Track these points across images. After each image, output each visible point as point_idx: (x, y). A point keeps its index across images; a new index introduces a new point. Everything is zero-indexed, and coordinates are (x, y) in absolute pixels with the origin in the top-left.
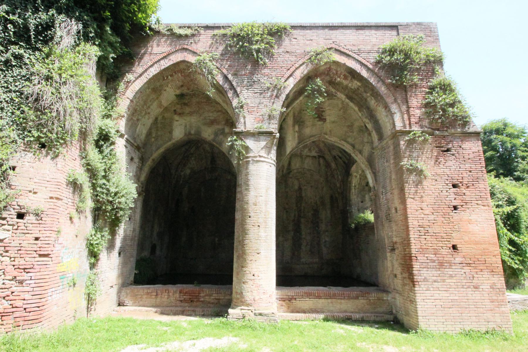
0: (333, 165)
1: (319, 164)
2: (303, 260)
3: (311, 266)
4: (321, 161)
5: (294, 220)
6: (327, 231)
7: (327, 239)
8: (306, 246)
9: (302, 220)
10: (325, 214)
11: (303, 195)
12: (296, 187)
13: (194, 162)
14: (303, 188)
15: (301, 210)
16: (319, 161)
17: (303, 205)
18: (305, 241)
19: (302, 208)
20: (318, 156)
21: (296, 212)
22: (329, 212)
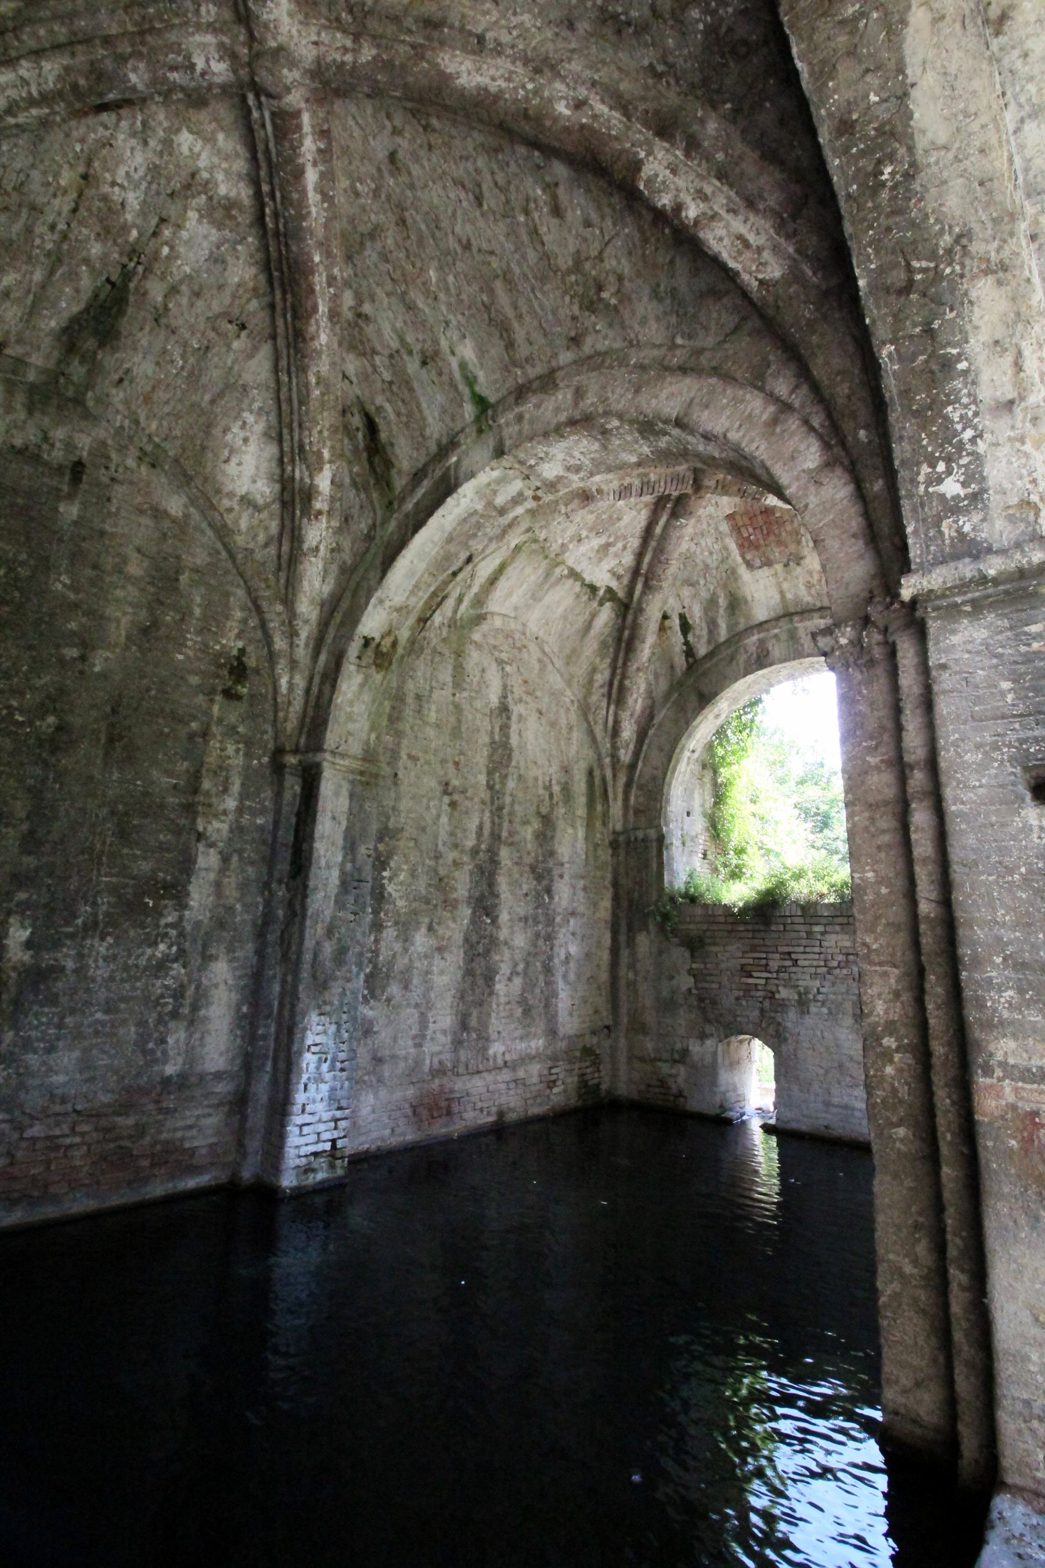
0: (646, 650)
1: (588, 626)
2: (496, 1049)
3: (521, 1073)
4: (606, 614)
5: (475, 852)
6: (573, 914)
7: (573, 949)
8: (510, 979)
9: (505, 854)
10: (572, 843)
11: (514, 741)
12: (494, 699)
14: (516, 709)
15: (501, 808)
16: (593, 616)
17: (511, 784)
18: (507, 953)
19: (508, 800)
20: (609, 590)
21: (487, 814)
22: (581, 833)
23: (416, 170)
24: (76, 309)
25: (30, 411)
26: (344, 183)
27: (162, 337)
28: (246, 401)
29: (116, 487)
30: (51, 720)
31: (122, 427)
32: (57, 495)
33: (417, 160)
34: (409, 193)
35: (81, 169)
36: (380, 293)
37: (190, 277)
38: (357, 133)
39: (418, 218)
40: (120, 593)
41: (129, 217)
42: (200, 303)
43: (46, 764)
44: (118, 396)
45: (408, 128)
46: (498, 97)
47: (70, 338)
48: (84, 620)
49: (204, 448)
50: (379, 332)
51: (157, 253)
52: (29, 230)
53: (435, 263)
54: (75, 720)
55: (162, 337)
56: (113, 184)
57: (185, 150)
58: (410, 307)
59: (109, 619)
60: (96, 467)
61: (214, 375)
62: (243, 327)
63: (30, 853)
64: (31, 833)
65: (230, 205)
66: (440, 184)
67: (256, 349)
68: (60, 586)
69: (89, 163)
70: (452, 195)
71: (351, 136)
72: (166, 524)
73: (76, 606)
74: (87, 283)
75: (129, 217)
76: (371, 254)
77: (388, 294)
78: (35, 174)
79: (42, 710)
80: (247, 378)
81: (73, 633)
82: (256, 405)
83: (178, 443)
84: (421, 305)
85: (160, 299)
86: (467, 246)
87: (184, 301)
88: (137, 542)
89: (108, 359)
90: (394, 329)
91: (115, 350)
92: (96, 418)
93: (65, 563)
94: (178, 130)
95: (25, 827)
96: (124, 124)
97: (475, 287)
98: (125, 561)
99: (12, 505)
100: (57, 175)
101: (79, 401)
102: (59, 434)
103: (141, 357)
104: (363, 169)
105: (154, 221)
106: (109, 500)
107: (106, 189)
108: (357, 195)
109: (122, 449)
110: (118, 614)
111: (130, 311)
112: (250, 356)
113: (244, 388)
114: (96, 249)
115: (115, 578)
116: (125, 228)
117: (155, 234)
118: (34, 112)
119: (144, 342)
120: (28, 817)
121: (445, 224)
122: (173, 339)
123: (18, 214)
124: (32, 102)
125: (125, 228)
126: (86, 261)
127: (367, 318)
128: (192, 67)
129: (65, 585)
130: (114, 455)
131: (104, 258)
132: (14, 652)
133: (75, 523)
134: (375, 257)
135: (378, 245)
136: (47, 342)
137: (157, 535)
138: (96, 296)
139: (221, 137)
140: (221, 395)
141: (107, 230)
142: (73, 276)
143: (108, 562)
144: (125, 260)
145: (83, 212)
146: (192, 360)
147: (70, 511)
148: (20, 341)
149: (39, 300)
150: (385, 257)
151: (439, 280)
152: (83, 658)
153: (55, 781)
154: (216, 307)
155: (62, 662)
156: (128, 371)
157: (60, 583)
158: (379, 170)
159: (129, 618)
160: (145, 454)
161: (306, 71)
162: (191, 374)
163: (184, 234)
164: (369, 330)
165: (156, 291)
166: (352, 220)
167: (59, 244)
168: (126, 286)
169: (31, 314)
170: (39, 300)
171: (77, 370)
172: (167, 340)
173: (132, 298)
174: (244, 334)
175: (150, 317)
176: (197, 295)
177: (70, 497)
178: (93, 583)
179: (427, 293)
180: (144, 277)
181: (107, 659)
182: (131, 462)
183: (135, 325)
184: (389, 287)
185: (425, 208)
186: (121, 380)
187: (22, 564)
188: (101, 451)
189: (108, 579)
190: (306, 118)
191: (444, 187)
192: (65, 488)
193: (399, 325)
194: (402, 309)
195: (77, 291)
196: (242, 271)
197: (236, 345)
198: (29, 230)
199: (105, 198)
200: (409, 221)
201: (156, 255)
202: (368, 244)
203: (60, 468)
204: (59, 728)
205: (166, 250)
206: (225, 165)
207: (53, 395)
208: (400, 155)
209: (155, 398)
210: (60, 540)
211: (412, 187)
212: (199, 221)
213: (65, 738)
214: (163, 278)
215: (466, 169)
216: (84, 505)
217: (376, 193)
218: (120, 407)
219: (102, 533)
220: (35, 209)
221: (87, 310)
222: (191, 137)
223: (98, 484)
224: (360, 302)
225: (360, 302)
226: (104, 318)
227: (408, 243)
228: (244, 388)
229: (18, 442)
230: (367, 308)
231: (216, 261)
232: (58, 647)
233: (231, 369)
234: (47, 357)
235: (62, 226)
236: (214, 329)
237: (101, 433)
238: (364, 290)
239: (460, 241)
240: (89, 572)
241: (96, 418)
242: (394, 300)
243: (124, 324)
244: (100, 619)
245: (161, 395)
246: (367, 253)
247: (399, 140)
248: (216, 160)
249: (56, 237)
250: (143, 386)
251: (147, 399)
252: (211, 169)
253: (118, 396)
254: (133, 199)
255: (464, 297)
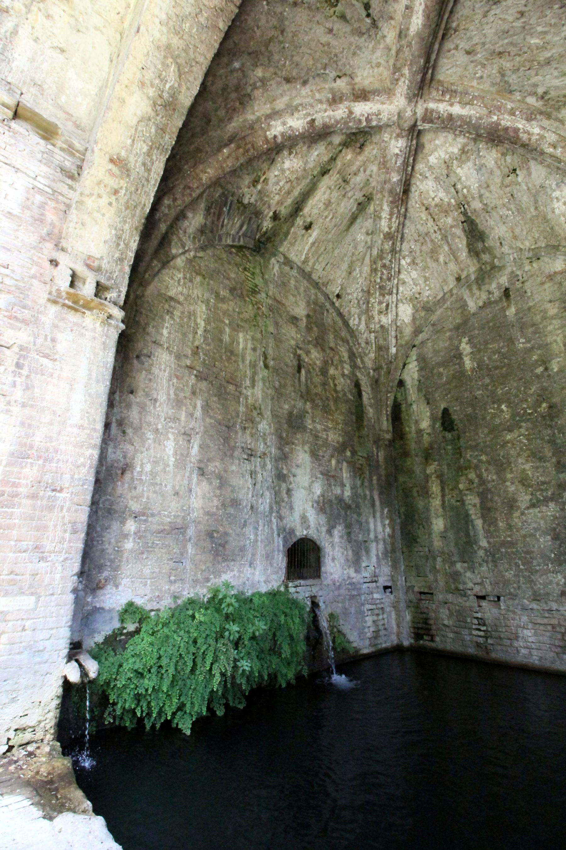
13: (414, 274)
23: (476, 40)
24: (465, 242)
25: (480, 289)
26: (475, 83)
27: (495, 214)
28: (549, 190)
29: (526, 284)
30: (544, 405)
31: (515, 259)
32: (503, 310)
33: (470, 38)
34: (487, 46)
35: (424, 208)
36: (534, 80)
37: (480, 186)
38: (454, 70)
39: (501, 43)
40: (550, 328)
41: (446, 200)
42: (492, 188)
43: (551, 426)
44: (506, 249)
45: (455, 41)
46: (426, 6)
47: (474, 252)
48: (539, 352)
49: (552, 228)
50: (557, 88)
51: (464, 195)
52: (432, 241)
53: (528, 37)
54: (556, 400)
55: (495, 214)
56: (433, 199)
57: (435, 161)
58: (548, 62)
59: (551, 343)
60: (514, 284)
61: (525, 199)
62: (515, 170)
63: (562, 472)
64: (559, 462)
65: (463, 151)
66: (485, 27)
67: (528, 169)
68: (521, 345)
69: (423, 204)
70: (492, 19)
71: (455, 73)
72: (558, 278)
73: (533, 348)
74: (459, 232)
75: (446, 200)
76: (513, 79)
77: (537, 75)
78: (419, 226)
79: (538, 403)
80: (538, 182)
81: (536, 361)
82: (554, 186)
83: (542, 238)
84: (549, 55)
85: (480, 205)
86: (522, 14)
87: (487, 194)
88: (548, 298)
89: (490, 243)
90: (556, 77)
91: (488, 238)
92: (504, 266)
93: (519, 334)
94: (428, 161)
95: (554, 460)
96: (418, 183)
97: (548, 12)
98: (545, 311)
99: (489, 328)
100: (421, 219)
101: (493, 267)
102: (494, 285)
103: (496, 230)
104: (471, 71)
105: (452, 190)
106: (526, 292)
107: (433, 204)
108: (481, 77)
109: (521, 267)
110: (555, 338)
111: (478, 221)
112: (530, 174)
113: (542, 187)
114: (450, 220)
115: (545, 323)
116: (449, 204)
117: (457, 192)
118: (394, 220)
119: (492, 223)
120: (553, 455)
121: (506, 27)
122: (498, 210)
123: (426, 241)
124: (390, 219)
125: (449, 204)
126: (452, 227)
127: (545, 93)
128: (397, 154)
129: (523, 343)
130: (519, 273)
131: (454, 219)
132: (515, 384)
133: (516, 314)
134: (514, 76)
135: (509, 73)
136: (469, 261)
137: (556, 287)
138: (465, 231)
139: (437, 142)
140: (536, 202)
141: (446, 211)
142: (454, 235)
143: (538, 318)
144: (460, 211)
145: (436, 217)
146: (512, 206)
147: (511, 311)
148: (462, 270)
149: (453, 253)
150: (516, 70)
151: (538, 38)
152: (546, 369)
153: (559, 433)
154: (498, 180)
155: (537, 376)
156: (499, 239)
157: (521, 344)
158: (472, 62)
159: (561, 336)
160: (531, 258)
161: (408, 104)
162: (518, 210)
163: (463, 178)
164: (553, 94)
165: (477, 205)
166: (493, 84)
167: (441, 234)
168: (469, 217)
169: (456, 260)
170: (453, 253)
171: (486, 257)
172: (498, 213)
173: (474, 218)
174: (518, 172)
175: (484, 214)
176: (488, 186)
177: (509, 306)
178: (535, 333)
179: (543, 48)
180: (469, 206)
181: (558, 362)
182: (527, 268)
183: (483, 223)
184: (533, 72)
185: (496, 38)
186: (501, 243)
187: (502, 348)
188: (514, 277)
189: (541, 326)
190: (432, 105)
191: (487, 24)
192: (505, 304)
193: (556, 73)
194: (547, 68)
195: (459, 237)
196: (491, 157)
197: (520, 179)
198: (432, 241)
199: (436, 205)
200: (501, 50)
201: (465, 197)
202: (506, 79)
203: (501, 299)
204: (550, 407)
205: (465, 191)
206: (447, 145)
207: (484, 276)
208: (467, 48)
209: (516, 234)
210: (513, 326)
211: (484, 44)
212: (462, 168)
213: (555, 410)
214: (473, 198)
215: (479, 8)
216: (516, 304)
217: (484, 66)
218: (511, 251)
219: (529, 309)
220: (427, 234)
221: (467, 238)
222: (432, 156)
223: (518, 290)
224: (535, 93)
225: (535, 93)
226: (475, 234)
227: (512, 54)
228: (542, 187)
229: (481, 304)
230: (540, 91)
231: (480, 169)
232: (532, 371)
233: (528, 189)
234: (474, 265)
235: (436, 228)
236: (506, 187)
237: (509, 270)
238: (529, 89)
239: (518, 19)
240: (531, 330)
241: (504, 266)
242: (541, 72)
243: (480, 227)
244: (546, 346)
245: (517, 231)
246: (511, 81)
247: (460, 47)
248: (444, 148)
249: (438, 232)
250: (508, 235)
251: (515, 238)
252: (447, 153)
253: (506, 249)
254: (441, 194)
255: (553, 21)
